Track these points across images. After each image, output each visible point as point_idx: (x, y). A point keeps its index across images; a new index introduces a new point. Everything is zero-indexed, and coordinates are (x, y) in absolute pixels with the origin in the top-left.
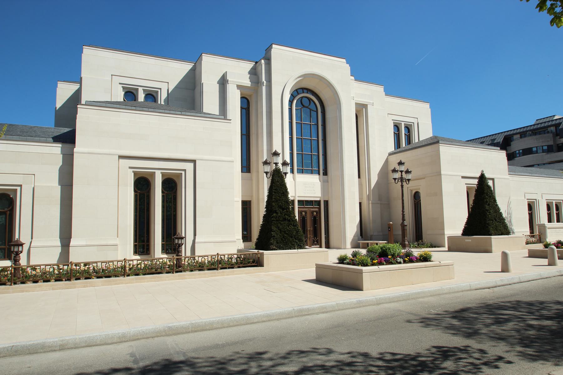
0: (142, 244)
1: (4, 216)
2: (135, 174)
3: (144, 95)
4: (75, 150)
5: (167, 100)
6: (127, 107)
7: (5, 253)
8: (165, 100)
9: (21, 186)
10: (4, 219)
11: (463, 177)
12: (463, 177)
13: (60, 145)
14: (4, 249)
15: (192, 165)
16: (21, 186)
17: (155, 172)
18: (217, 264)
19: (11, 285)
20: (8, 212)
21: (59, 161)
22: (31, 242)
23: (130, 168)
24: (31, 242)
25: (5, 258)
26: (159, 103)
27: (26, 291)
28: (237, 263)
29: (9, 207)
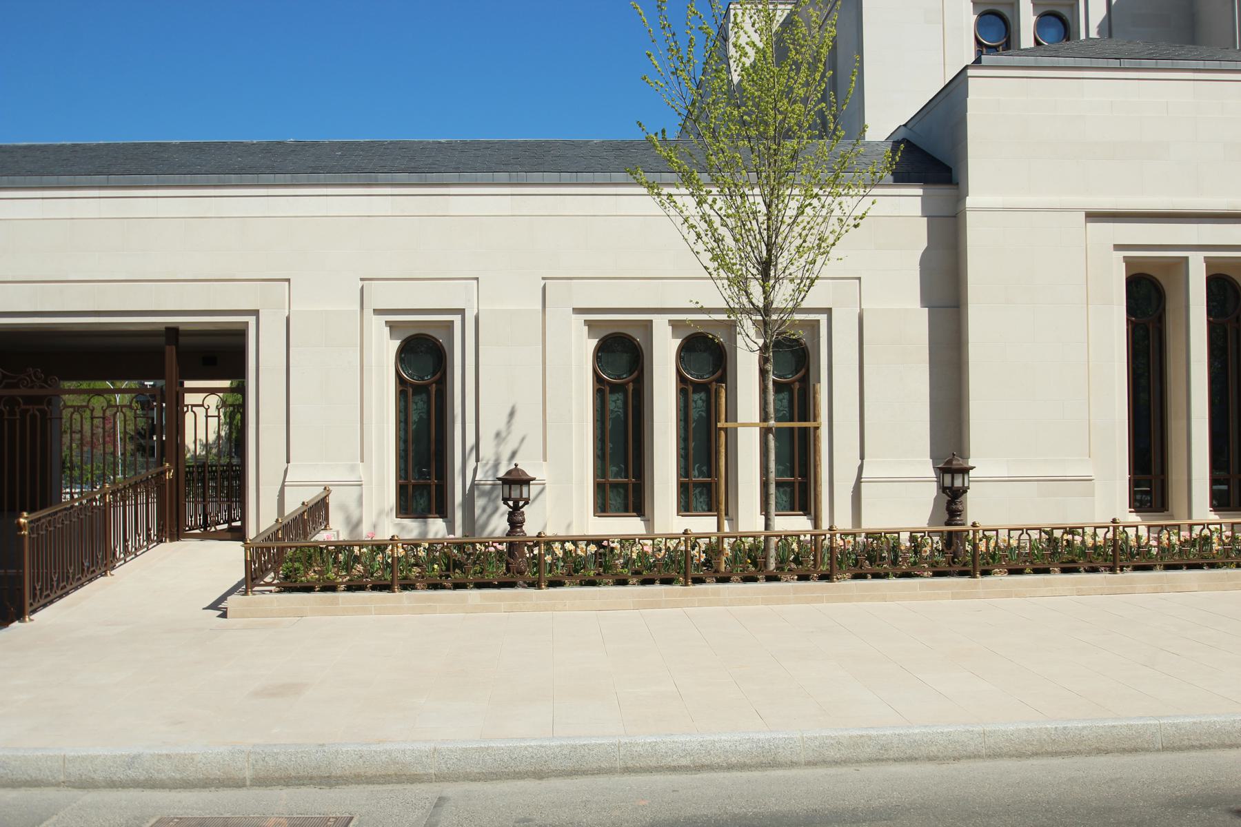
0: (1150, 480)
1: (424, 396)
2: (1129, 262)
3: (1033, 19)
4: (970, 201)
5: (1108, 27)
6: (1162, 64)
7: (626, 497)
8: (1100, 26)
9: (828, 311)
10: (620, 403)
11: (1093, 216)
12: (1093, 216)
13: (920, 191)
14: (625, 486)
15: (459, 317)
16: (828, 311)
17: (1187, 258)
18: (1058, 555)
19: (686, 584)
20: (797, 385)
21: (918, 235)
22: (861, 468)
23: (1118, 247)
24: (861, 468)
25: (626, 510)
26: (1083, 36)
27: (1017, 596)
28: (1226, 553)
29: (434, 374)
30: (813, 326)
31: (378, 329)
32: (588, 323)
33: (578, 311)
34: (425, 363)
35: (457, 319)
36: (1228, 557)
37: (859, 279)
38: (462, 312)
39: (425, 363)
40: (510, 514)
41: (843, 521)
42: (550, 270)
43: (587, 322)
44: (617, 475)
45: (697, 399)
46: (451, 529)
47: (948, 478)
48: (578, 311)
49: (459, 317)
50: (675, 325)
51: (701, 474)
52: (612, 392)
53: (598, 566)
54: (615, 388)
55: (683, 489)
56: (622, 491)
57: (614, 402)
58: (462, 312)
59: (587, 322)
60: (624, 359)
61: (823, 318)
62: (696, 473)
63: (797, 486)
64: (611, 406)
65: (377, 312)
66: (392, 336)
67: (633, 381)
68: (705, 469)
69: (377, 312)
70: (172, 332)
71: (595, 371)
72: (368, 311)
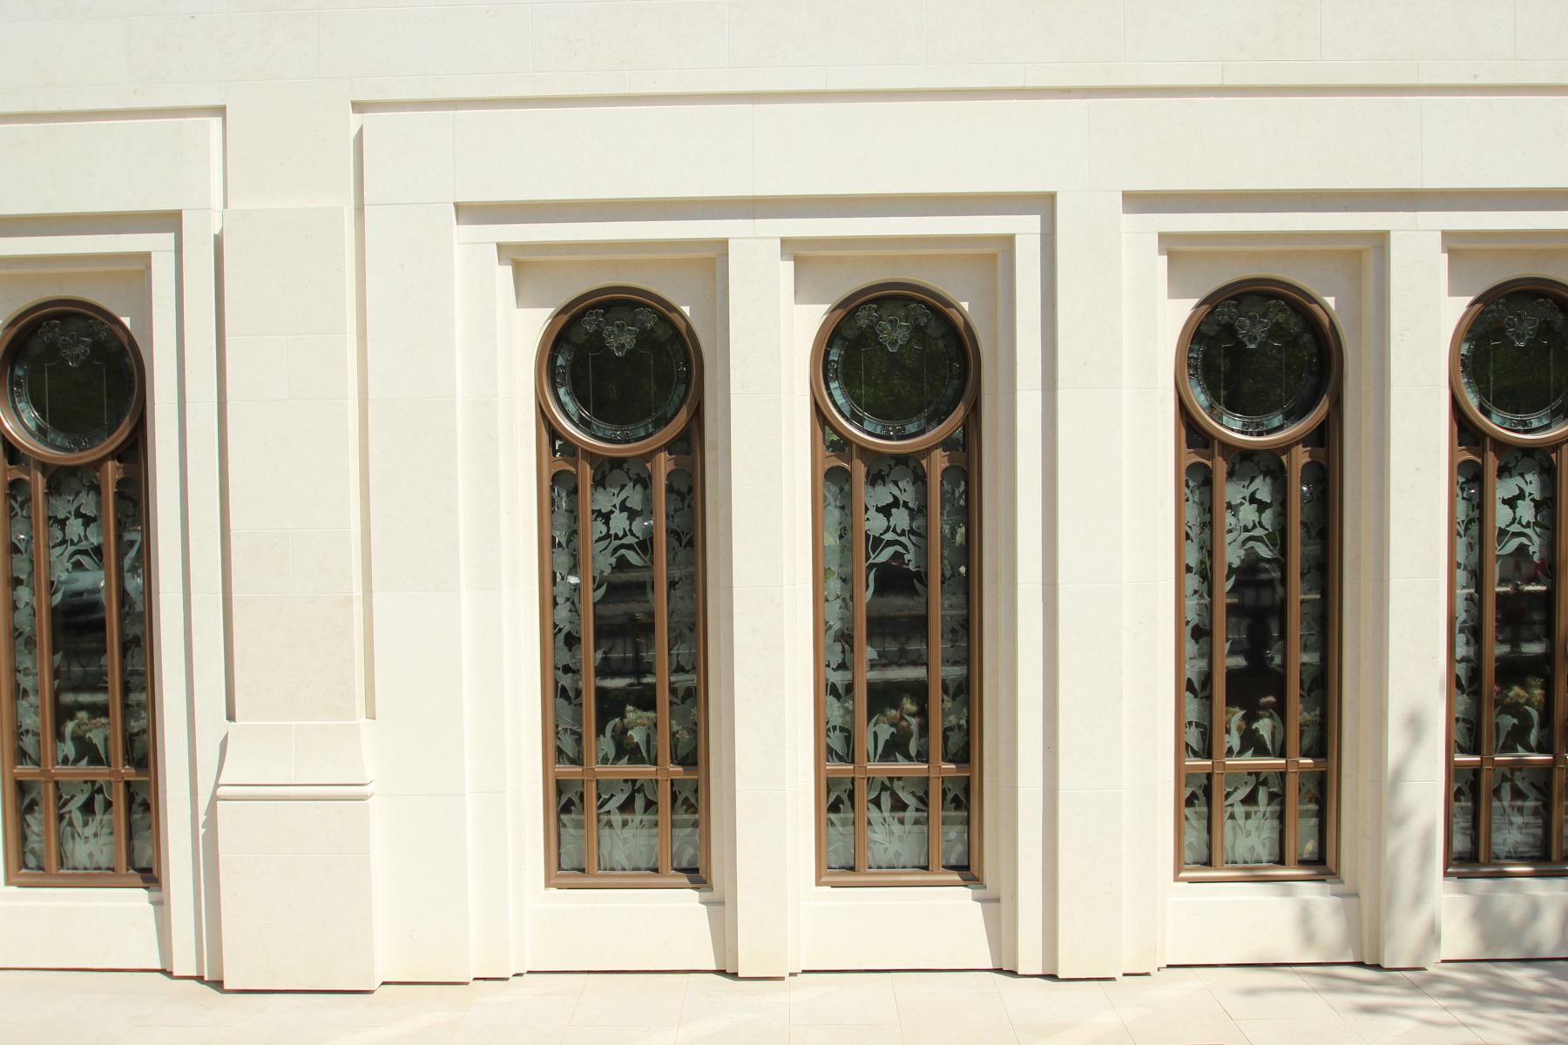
9: (1044, 205)
31: (474, 272)
35: (158, 245)
38: (170, 221)
43: (505, 251)
48: (469, 213)
57: (1243, 510)
59: (505, 251)
66: (524, 292)
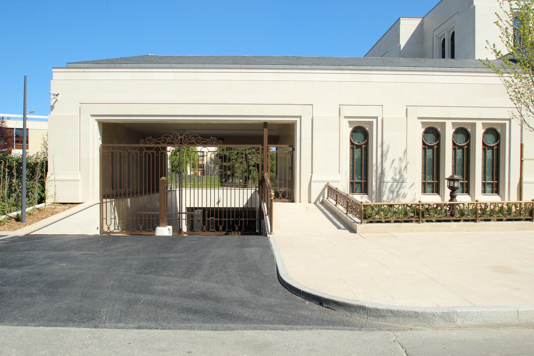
9: (300, 117)
10: (431, 153)
15: (375, 120)
16: (300, 117)
30: (370, 124)
32: (422, 123)
33: (419, 118)
34: (361, 137)
35: (374, 121)
36: (520, 214)
37: (312, 105)
38: (377, 118)
39: (361, 137)
40: (451, 192)
41: (514, 198)
42: (406, 103)
44: (429, 179)
45: (357, 152)
46: (443, 198)
47: (452, 183)
49: (375, 120)
50: (453, 124)
51: (358, 179)
52: (428, 149)
53: (418, 214)
54: (358, 147)
55: (484, 185)
56: (431, 185)
58: (377, 118)
60: (360, 136)
61: (507, 122)
62: (356, 178)
63: (494, 184)
64: (428, 154)
65: (345, 117)
66: (350, 127)
67: (364, 144)
68: (360, 177)
69: (345, 117)
70: (265, 124)
71: (423, 141)
72: (342, 117)
